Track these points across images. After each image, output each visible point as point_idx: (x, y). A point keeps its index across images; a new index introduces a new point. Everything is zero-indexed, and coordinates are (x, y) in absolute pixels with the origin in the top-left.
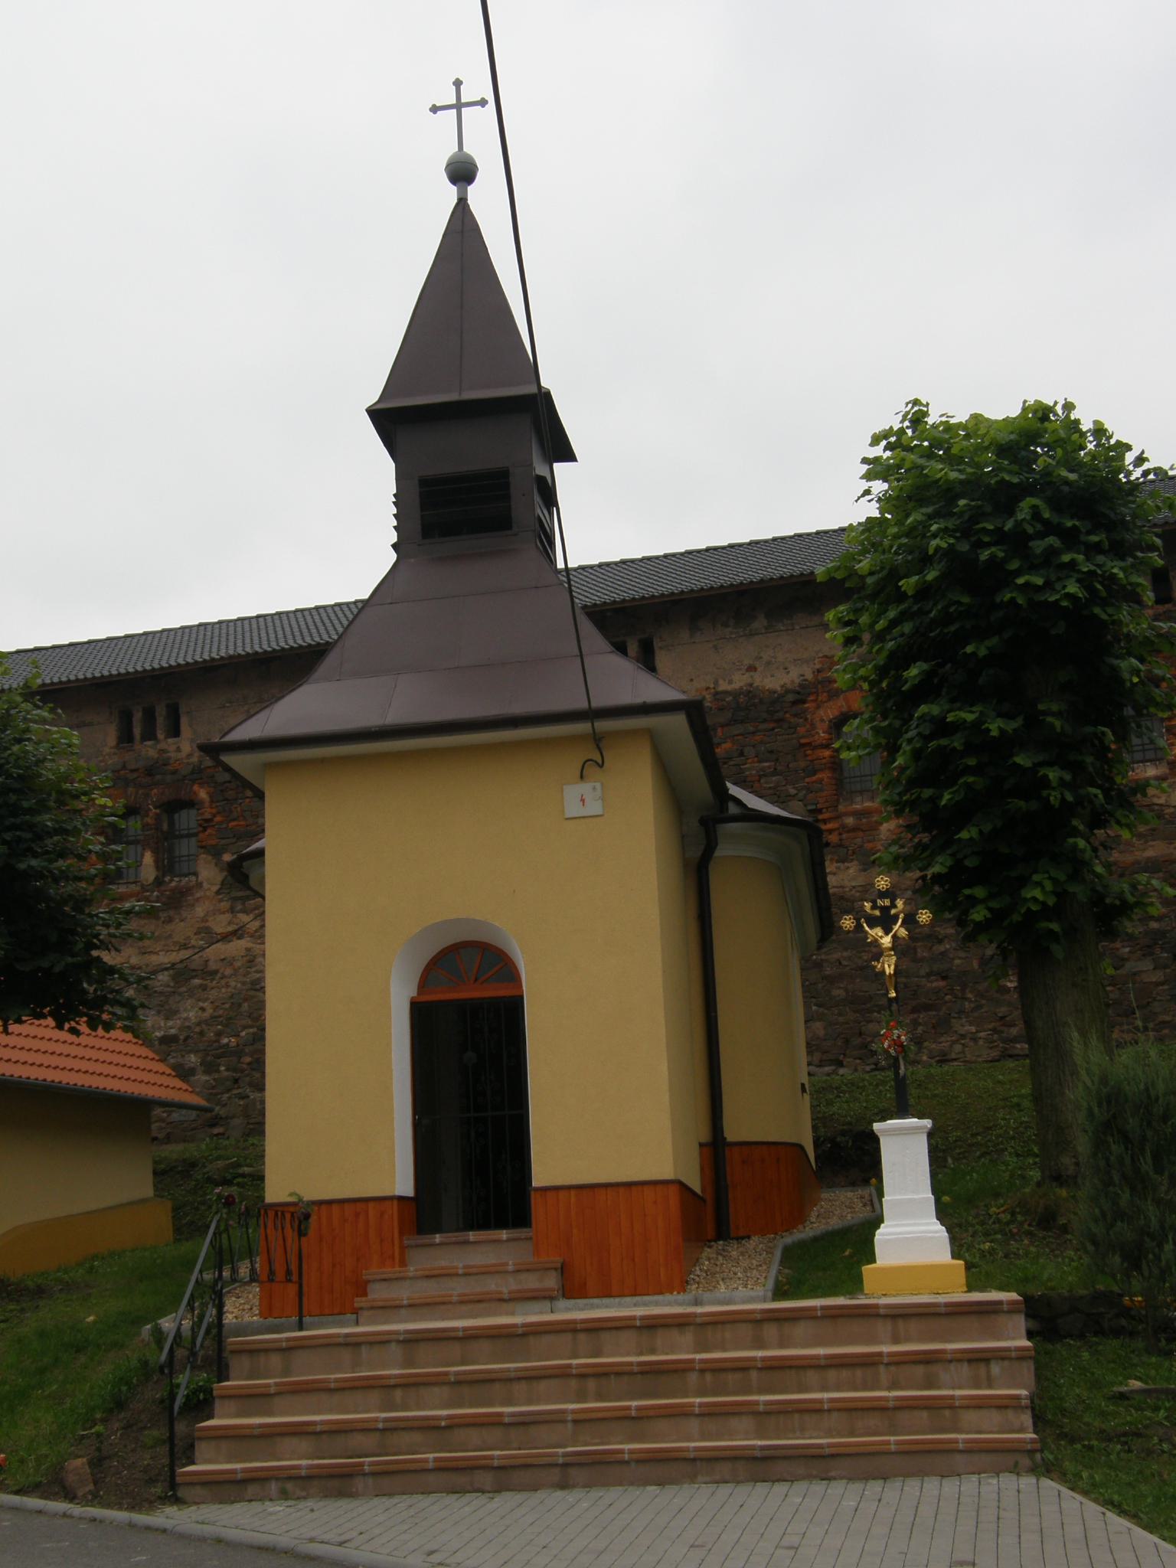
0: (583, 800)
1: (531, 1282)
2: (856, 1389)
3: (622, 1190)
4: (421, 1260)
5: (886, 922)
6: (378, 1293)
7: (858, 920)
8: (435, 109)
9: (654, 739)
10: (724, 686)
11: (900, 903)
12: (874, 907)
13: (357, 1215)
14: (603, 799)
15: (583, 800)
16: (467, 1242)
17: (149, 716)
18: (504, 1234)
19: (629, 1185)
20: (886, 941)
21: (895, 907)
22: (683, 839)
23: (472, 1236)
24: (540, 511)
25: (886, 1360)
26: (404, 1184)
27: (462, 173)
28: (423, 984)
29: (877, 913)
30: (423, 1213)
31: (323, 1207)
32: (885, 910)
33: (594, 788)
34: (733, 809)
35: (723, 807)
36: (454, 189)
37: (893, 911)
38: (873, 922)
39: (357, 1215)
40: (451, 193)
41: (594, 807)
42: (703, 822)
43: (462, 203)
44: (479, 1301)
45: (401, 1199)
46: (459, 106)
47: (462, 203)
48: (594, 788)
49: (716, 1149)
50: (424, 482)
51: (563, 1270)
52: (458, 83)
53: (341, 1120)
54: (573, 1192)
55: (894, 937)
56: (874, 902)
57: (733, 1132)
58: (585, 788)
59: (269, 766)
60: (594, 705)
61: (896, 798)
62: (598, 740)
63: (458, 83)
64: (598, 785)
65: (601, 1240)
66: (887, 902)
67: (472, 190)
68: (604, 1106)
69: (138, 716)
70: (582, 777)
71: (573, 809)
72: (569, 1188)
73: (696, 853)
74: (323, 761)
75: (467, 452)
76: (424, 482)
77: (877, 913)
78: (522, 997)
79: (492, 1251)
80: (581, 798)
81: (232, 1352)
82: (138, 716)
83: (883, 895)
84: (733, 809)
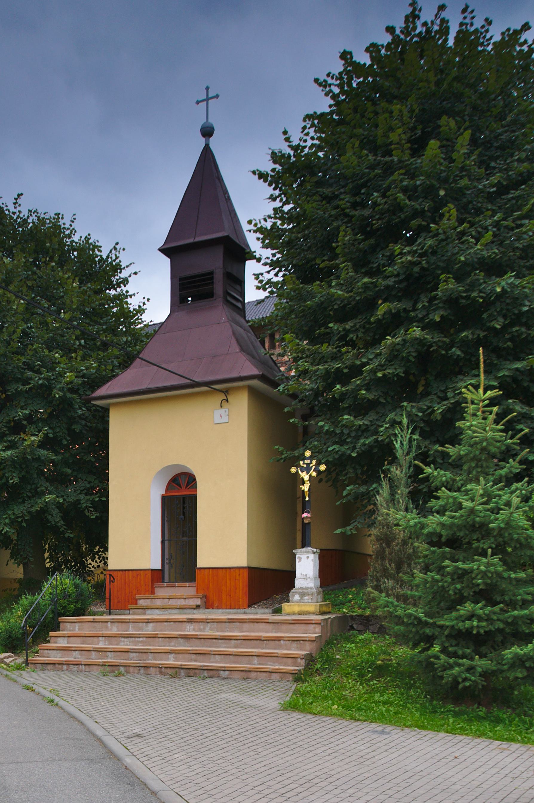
3: (228, 570)
4: (160, 592)
5: (307, 469)
6: (142, 603)
12: (304, 464)
13: (137, 575)
14: (228, 415)
18: (187, 584)
19: (230, 568)
23: (177, 584)
27: (207, 132)
29: (305, 466)
36: (203, 140)
37: (311, 465)
39: (137, 575)
40: (202, 142)
41: (225, 419)
46: (207, 100)
52: (207, 89)
55: (310, 475)
58: (222, 411)
60: (138, 360)
62: (226, 392)
63: (207, 89)
64: (227, 410)
65: (215, 589)
67: (213, 142)
68: (227, 537)
71: (217, 420)
72: (209, 568)
76: (181, 279)
79: (186, 591)
80: (220, 415)
81: (320, 624)
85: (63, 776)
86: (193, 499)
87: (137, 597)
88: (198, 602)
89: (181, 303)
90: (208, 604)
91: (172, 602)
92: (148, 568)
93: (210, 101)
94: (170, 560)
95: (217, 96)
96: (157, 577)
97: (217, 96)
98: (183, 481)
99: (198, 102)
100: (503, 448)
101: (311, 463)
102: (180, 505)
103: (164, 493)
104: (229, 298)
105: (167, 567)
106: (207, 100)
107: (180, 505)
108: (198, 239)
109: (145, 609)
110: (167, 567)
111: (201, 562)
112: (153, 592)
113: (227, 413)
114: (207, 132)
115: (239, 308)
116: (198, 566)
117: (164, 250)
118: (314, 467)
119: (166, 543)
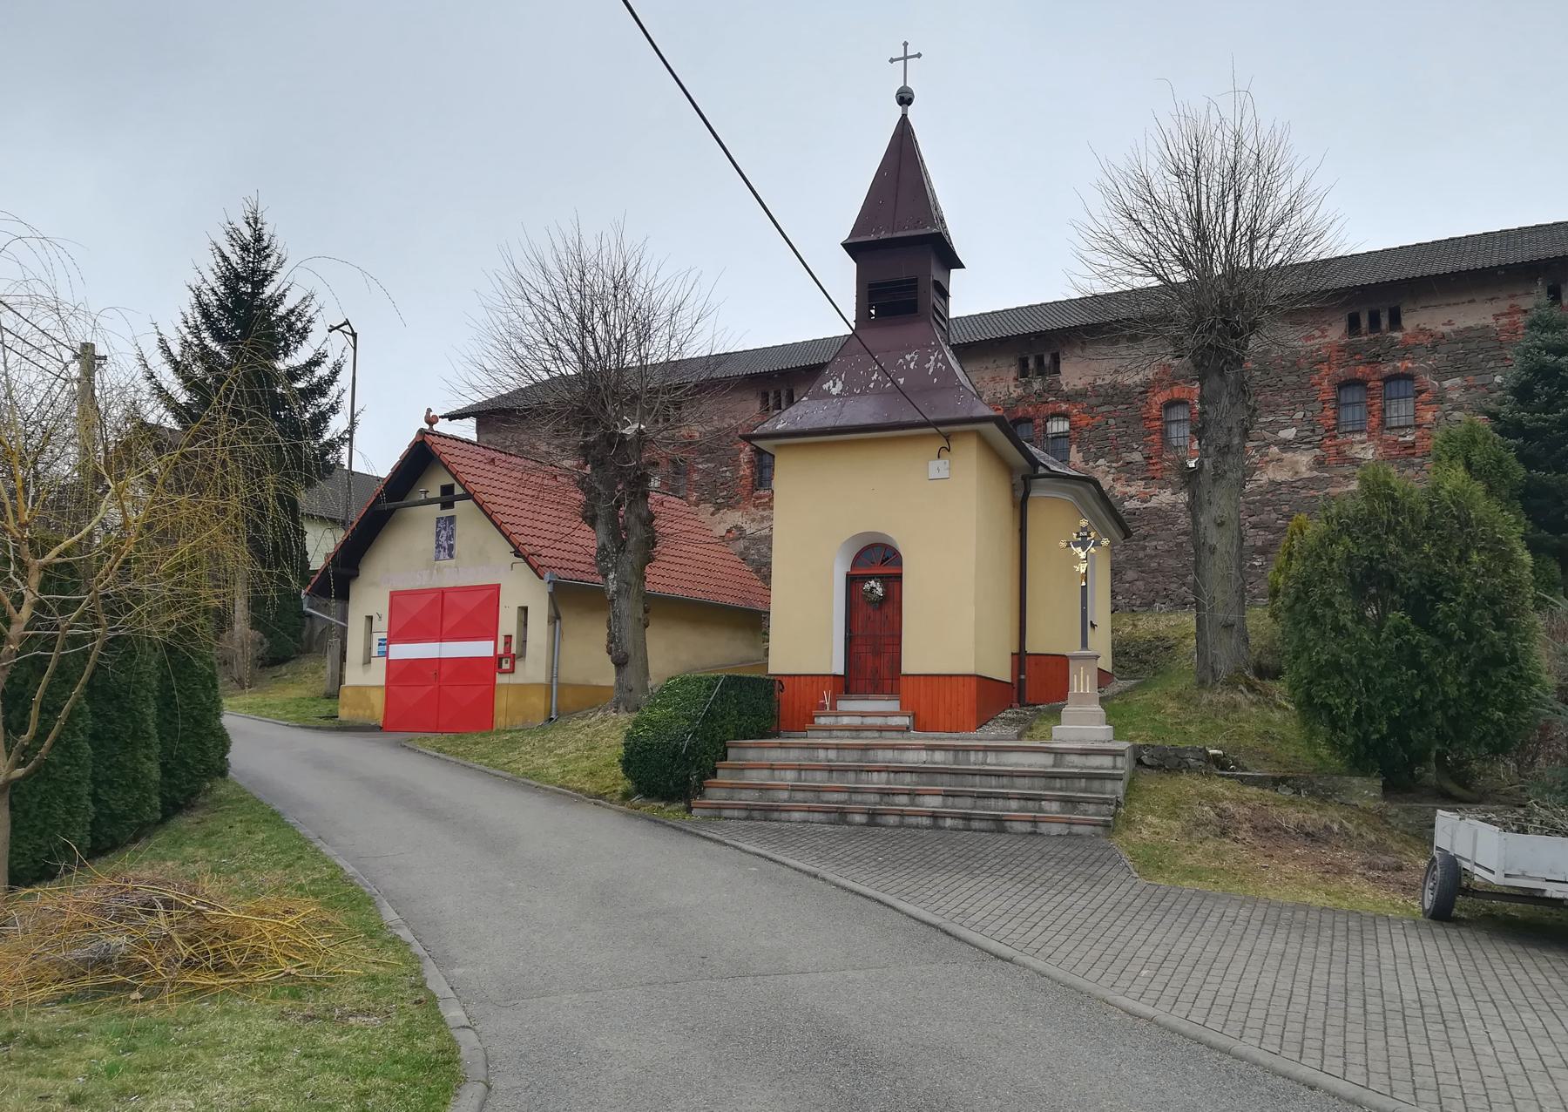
8: (892, 61)
9: (979, 434)
10: (1099, 382)
17: (778, 395)
19: (951, 676)
20: (1083, 555)
22: (1013, 488)
24: (935, 299)
26: (838, 668)
27: (905, 99)
28: (853, 566)
30: (848, 684)
34: (1042, 471)
35: (1036, 470)
38: (1076, 544)
40: (898, 111)
42: (1023, 478)
45: (835, 676)
46: (906, 58)
47: (904, 117)
49: (1021, 658)
50: (870, 286)
51: (915, 716)
52: (906, 44)
53: (806, 634)
57: (1029, 649)
58: (940, 463)
59: (778, 447)
61: (1492, 406)
62: (947, 437)
63: (906, 44)
67: (912, 111)
68: (949, 630)
69: (772, 395)
71: (933, 474)
73: (1020, 494)
74: (798, 445)
75: (895, 269)
76: (870, 286)
80: (938, 468)
82: (772, 395)
83: (1084, 529)
84: (1042, 471)
87: (815, 712)
88: (906, 721)
90: (919, 725)
91: (869, 721)
100: (1381, 478)
102: (875, 578)
106: (906, 58)
107: (875, 578)
108: (899, 234)
109: (829, 729)
114: (905, 99)
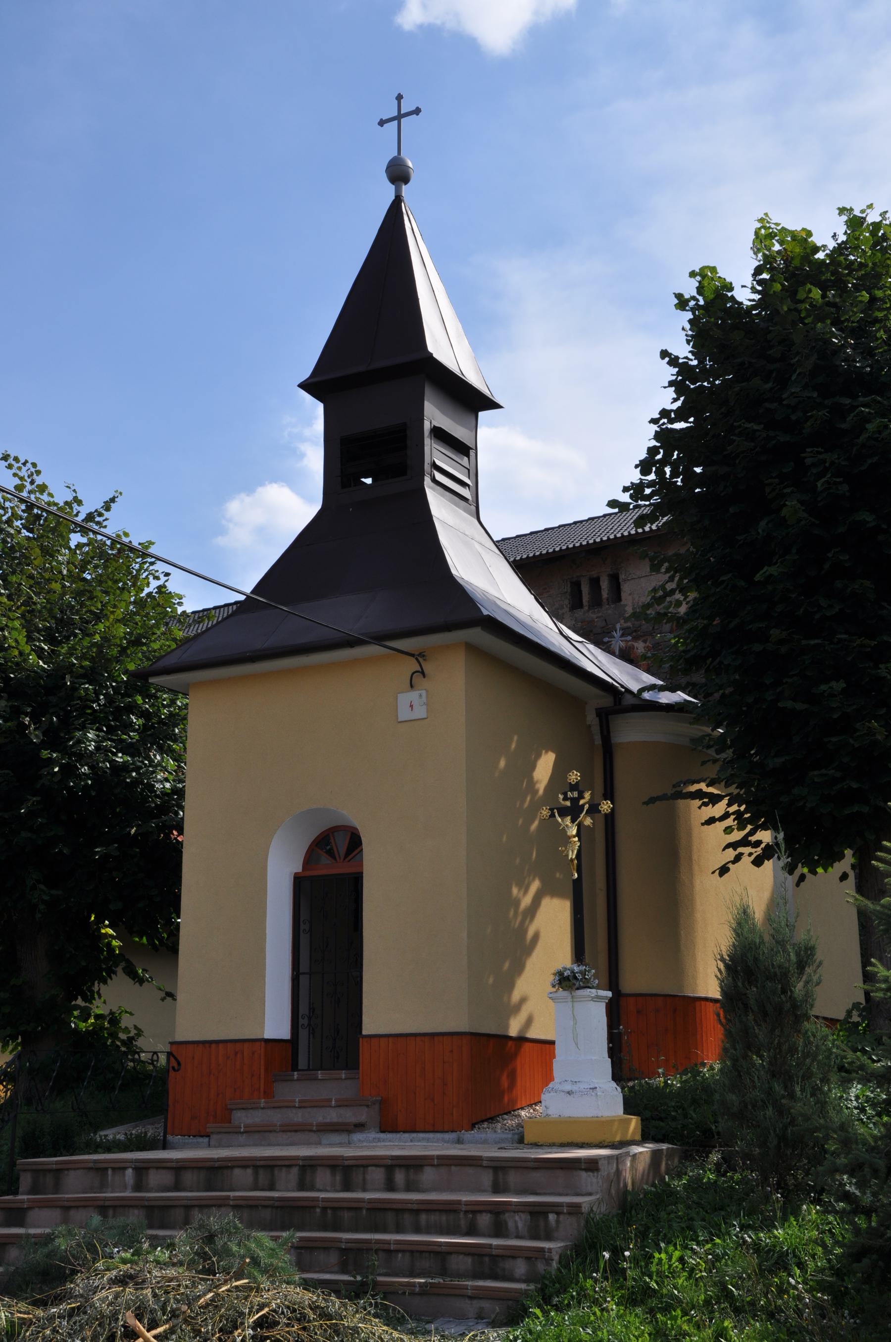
0: (411, 706)
1: (349, 1116)
2: (325, 1229)
7: (552, 810)
11: (587, 795)
12: (565, 799)
13: (236, 1054)
14: (427, 704)
15: (411, 706)
16: (316, 1079)
19: (433, 1035)
21: (583, 798)
23: (320, 1074)
25: (464, 1208)
27: (398, 174)
28: (309, 859)
31: (221, 1045)
32: (575, 801)
33: (421, 696)
36: (392, 188)
37: (582, 802)
38: (563, 812)
39: (236, 1054)
40: (388, 192)
41: (420, 712)
43: (398, 201)
44: (296, 1131)
46: (399, 117)
48: (421, 696)
52: (399, 98)
54: (391, 1039)
56: (565, 794)
58: (413, 696)
63: (399, 98)
64: (424, 693)
66: (576, 794)
67: (406, 190)
70: (412, 686)
71: (404, 714)
77: (568, 803)
78: (362, 873)
79: (332, 1086)
80: (411, 704)
83: (573, 787)
85: (681, 1260)
86: (356, 881)
89: (344, 486)
92: (197, 1039)
93: (396, 114)
94: (310, 1018)
95: (417, 111)
96: (281, 1057)
97: (417, 111)
98: (341, 844)
99: (382, 123)
101: (581, 796)
103: (300, 870)
104: (439, 477)
105: (303, 1034)
106: (399, 117)
110: (303, 1034)
111: (374, 1021)
112: (268, 1094)
113: (424, 699)
115: (465, 499)
116: (364, 1032)
117: (312, 387)
118: (587, 806)
119: (304, 980)
